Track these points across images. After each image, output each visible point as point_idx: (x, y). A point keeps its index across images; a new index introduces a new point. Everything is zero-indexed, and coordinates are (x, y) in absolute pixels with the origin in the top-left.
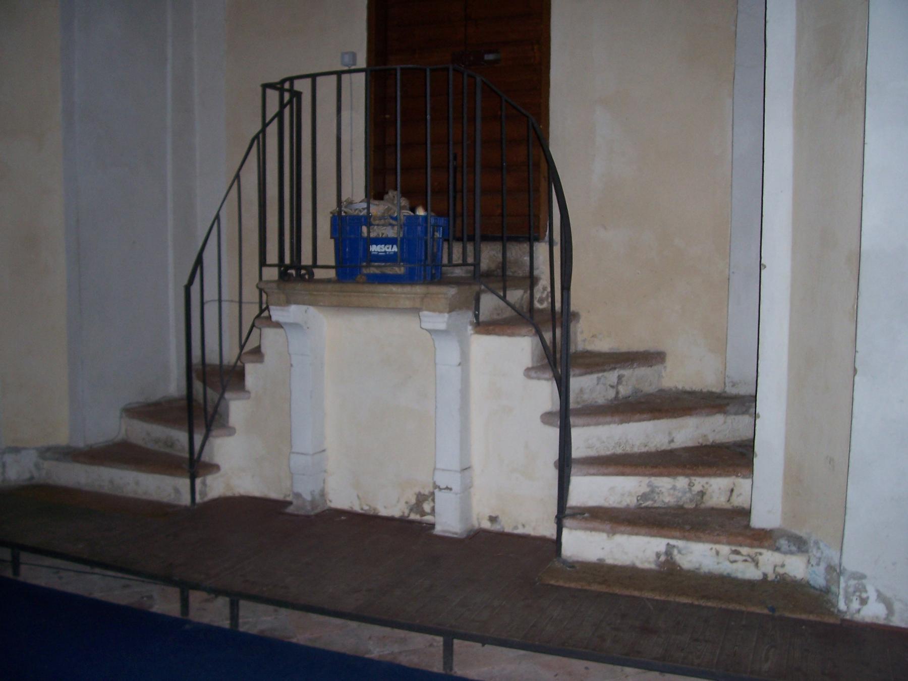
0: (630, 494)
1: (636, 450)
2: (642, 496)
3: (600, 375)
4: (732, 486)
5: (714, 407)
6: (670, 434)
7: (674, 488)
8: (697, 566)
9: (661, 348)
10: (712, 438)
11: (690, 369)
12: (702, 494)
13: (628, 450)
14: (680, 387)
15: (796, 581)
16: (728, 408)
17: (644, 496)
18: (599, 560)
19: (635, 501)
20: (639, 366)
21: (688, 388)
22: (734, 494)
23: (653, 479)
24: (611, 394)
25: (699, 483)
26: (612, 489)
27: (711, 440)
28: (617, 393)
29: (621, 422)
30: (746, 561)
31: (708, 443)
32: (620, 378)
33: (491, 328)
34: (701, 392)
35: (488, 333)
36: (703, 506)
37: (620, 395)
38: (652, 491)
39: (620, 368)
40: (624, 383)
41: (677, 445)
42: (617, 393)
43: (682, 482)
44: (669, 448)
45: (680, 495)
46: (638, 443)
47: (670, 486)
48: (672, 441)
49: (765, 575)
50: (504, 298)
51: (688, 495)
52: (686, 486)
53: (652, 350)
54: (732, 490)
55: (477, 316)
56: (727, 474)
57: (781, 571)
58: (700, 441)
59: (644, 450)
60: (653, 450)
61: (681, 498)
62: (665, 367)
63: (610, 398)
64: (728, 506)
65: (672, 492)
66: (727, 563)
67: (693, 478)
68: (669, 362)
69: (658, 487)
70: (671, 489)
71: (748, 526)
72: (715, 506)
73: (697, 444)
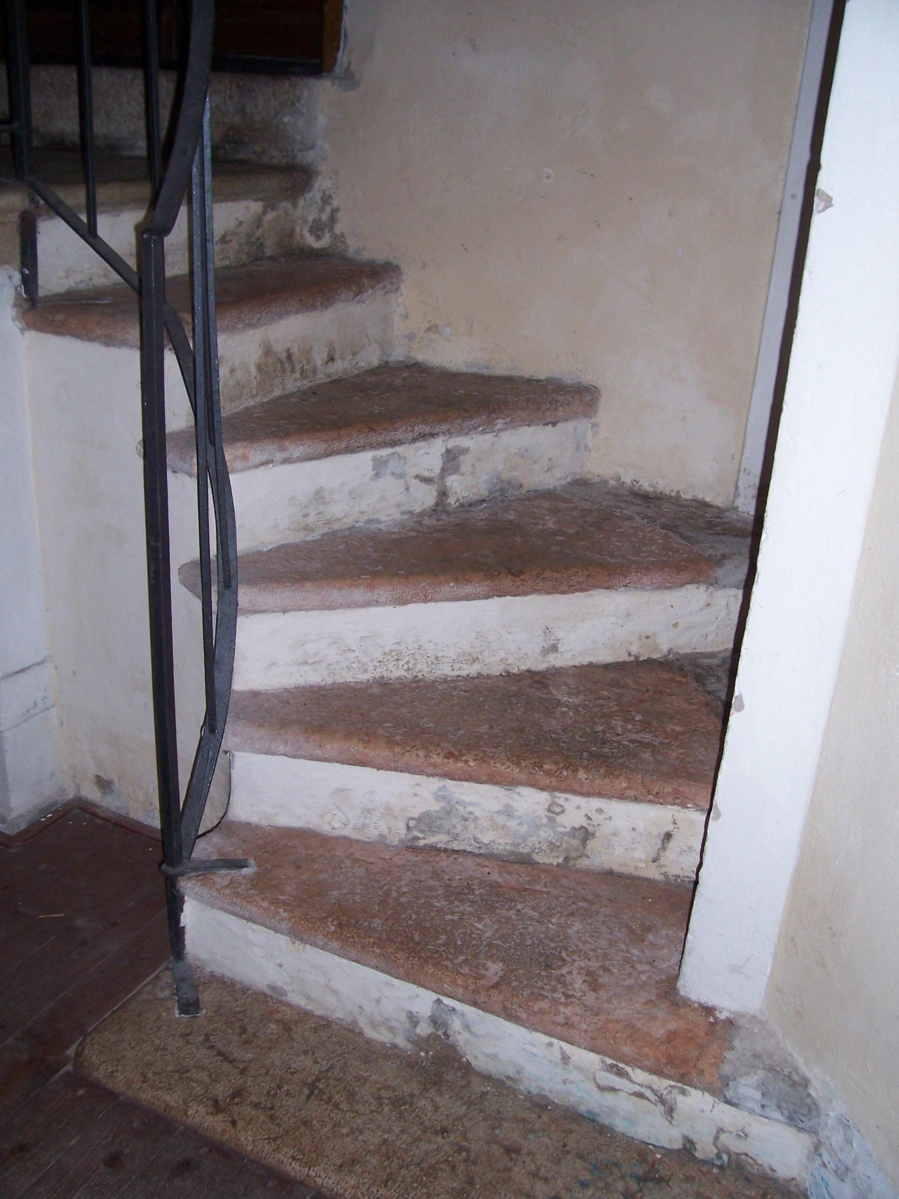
0: (388, 810)
1: (445, 670)
2: (419, 820)
3: (384, 452)
4: (669, 828)
5: (678, 568)
6: (547, 630)
7: (508, 811)
8: (511, 1072)
9: (588, 378)
10: (666, 643)
11: (652, 436)
12: (585, 834)
13: (423, 670)
14: (627, 480)
15: (774, 1180)
16: (720, 572)
17: (427, 821)
18: (271, 987)
19: (403, 830)
20: (513, 424)
21: (646, 486)
22: (673, 844)
23: (449, 783)
24: (425, 497)
25: (576, 809)
26: (341, 791)
27: (664, 648)
28: (443, 494)
29: (402, 601)
30: (640, 1095)
31: (655, 656)
32: (452, 458)
33: (59, 317)
34: (677, 500)
35: (58, 330)
36: (583, 863)
37: (452, 500)
38: (448, 812)
39: (450, 433)
40: (465, 468)
41: (563, 660)
42: (443, 494)
43: (530, 801)
44: (542, 667)
45: (524, 829)
46: (452, 654)
47: (496, 806)
48: (554, 648)
49: (689, 1146)
50: (89, 233)
51: (545, 834)
52: (542, 812)
53: (568, 380)
54: (668, 836)
55: (30, 281)
56: (657, 798)
57: (737, 1146)
58: (634, 649)
59: (472, 670)
60: (496, 670)
61: (524, 838)
62: (595, 425)
63: (417, 509)
64: (653, 873)
65: (501, 820)
66: (590, 1086)
67: (561, 798)
68: (607, 411)
69: (465, 805)
70: (504, 813)
71: (668, 989)
72: (616, 868)
73: (624, 657)
